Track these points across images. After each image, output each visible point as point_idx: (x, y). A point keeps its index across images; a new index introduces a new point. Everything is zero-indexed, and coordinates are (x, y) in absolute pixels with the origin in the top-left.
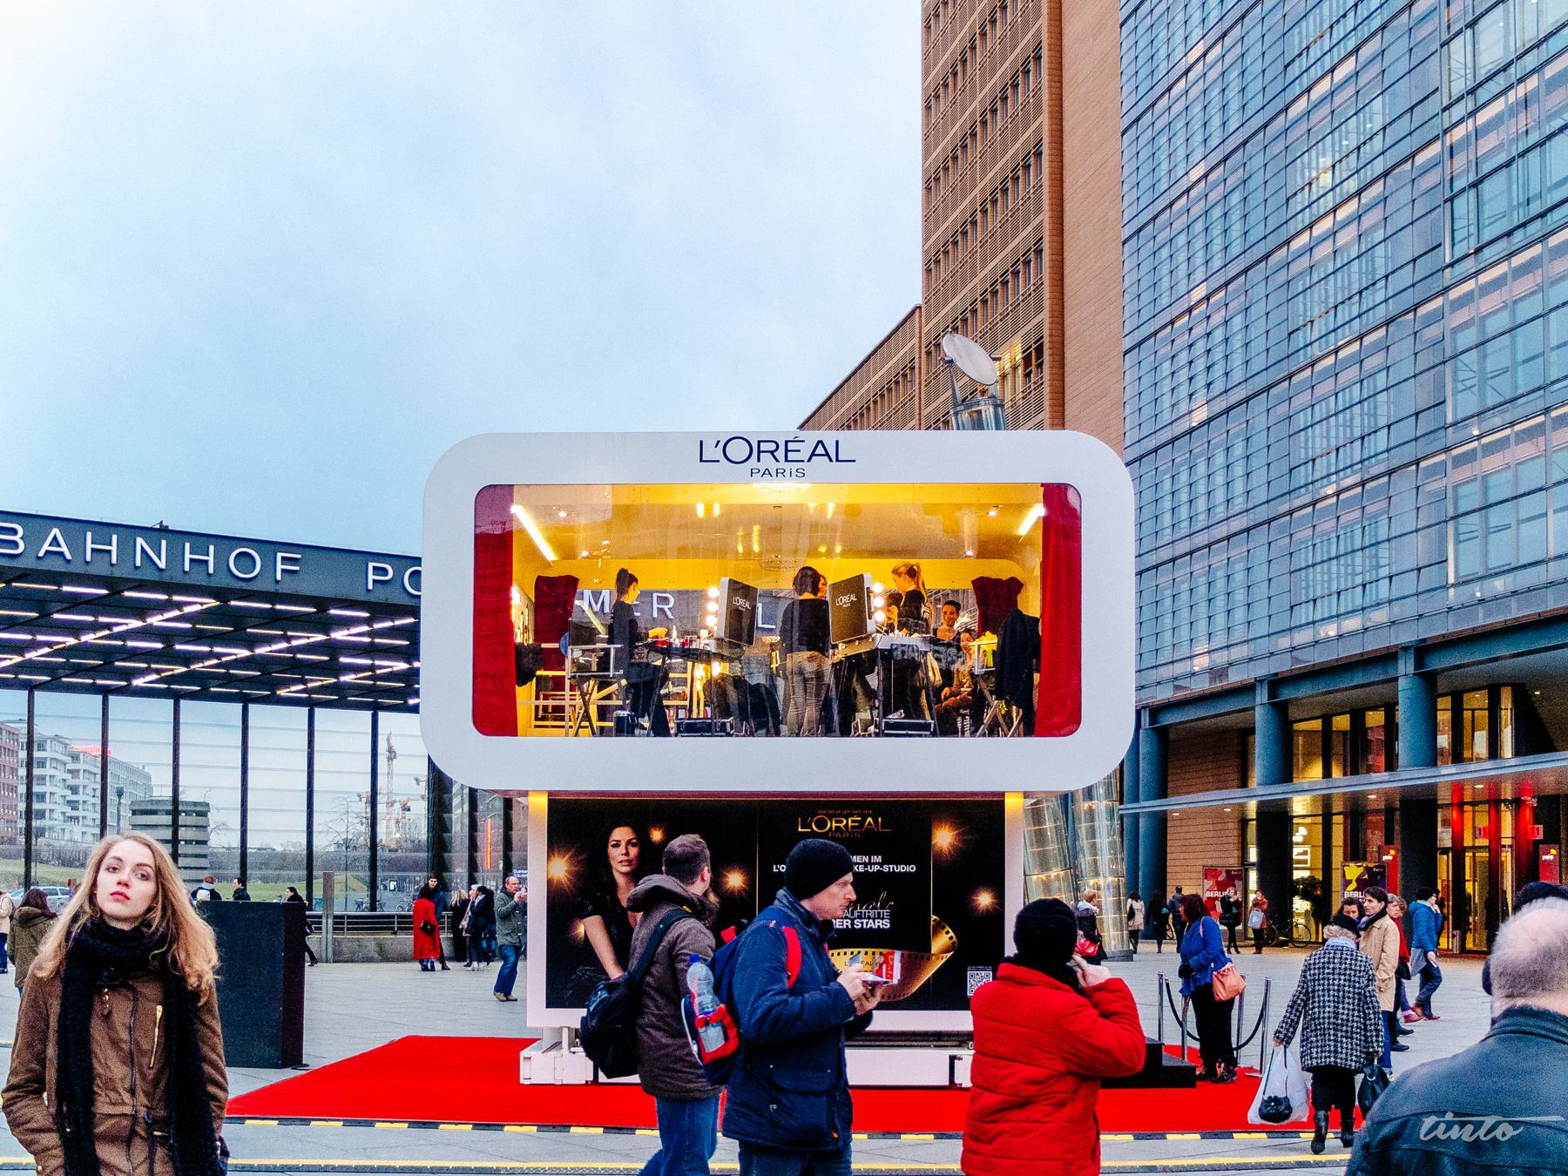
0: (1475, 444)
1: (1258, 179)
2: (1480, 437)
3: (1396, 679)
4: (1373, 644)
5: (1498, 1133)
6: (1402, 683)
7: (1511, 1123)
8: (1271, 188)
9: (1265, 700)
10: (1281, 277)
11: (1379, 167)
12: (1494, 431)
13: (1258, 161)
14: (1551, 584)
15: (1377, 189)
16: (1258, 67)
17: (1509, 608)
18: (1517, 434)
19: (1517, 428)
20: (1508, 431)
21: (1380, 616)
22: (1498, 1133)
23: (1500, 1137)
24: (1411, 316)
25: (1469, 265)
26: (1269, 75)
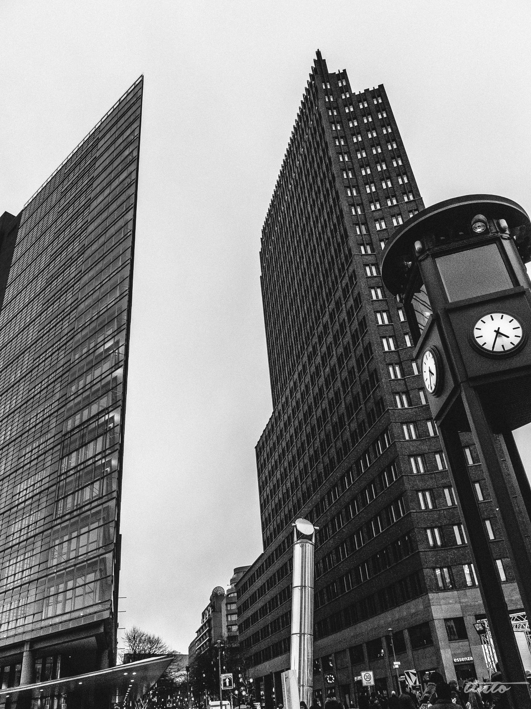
0: (54, 575)
1: (5, 490)
2: (56, 572)
3: (23, 653)
4: (17, 640)
5: (499, 690)
6: (25, 654)
7: (505, 685)
8: (9, 493)
9: (28, 649)
10: (7, 520)
11: (38, 491)
12: (60, 571)
13: (6, 484)
14: (42, 628)
15: (37, 497)
16: (11, 458)
17: (93, 618)
18: (67, 572)
19: (67, 570)
20: (64, 571)
21: (20, 630)
22: (499, 690)
23: (500, 692)
24: (41, 534)
25: (59, 521)
26: (14, 461)
